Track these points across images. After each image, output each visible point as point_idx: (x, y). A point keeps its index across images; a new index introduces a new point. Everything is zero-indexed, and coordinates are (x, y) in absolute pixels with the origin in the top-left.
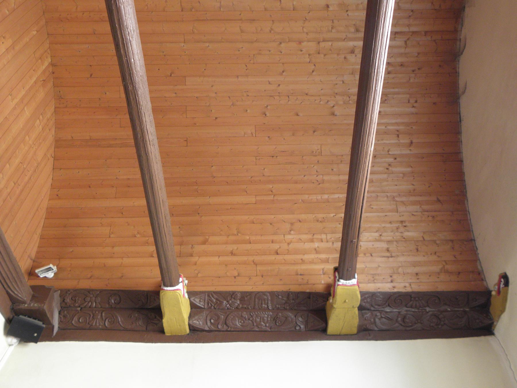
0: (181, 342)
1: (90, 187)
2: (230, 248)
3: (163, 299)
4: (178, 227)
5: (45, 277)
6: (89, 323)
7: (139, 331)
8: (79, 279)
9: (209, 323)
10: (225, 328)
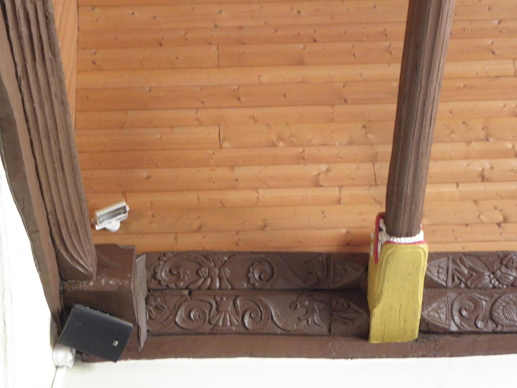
0: (405, 356)
1: (161, 45)
2: (478, 165)
3: (387, 262)
4: (360, 125)
5: (105, 229)
6: (209, 322)
7: (315, 335)
8: (176, 233)
9: (457, 318)
10: (491, 326)
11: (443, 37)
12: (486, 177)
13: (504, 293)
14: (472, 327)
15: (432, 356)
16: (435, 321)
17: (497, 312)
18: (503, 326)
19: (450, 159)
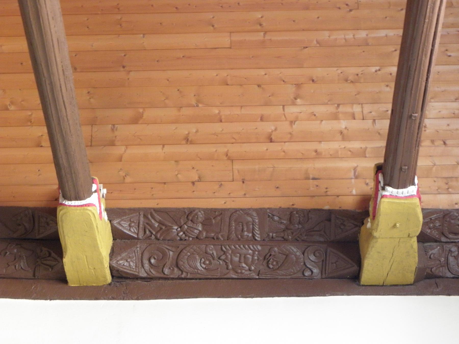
0: (97, 299)
2: (184, 129)
4: (85, 91)
9: (147, 266)
10: (177, 273)
11: (50, 36)
12: (190, 139)
13: (189, 245)
14: (160, 273)
15: (120, 299)
16: (125, 269)
17: (182, 261)
18: (187, 273)
19: (161, 123)
